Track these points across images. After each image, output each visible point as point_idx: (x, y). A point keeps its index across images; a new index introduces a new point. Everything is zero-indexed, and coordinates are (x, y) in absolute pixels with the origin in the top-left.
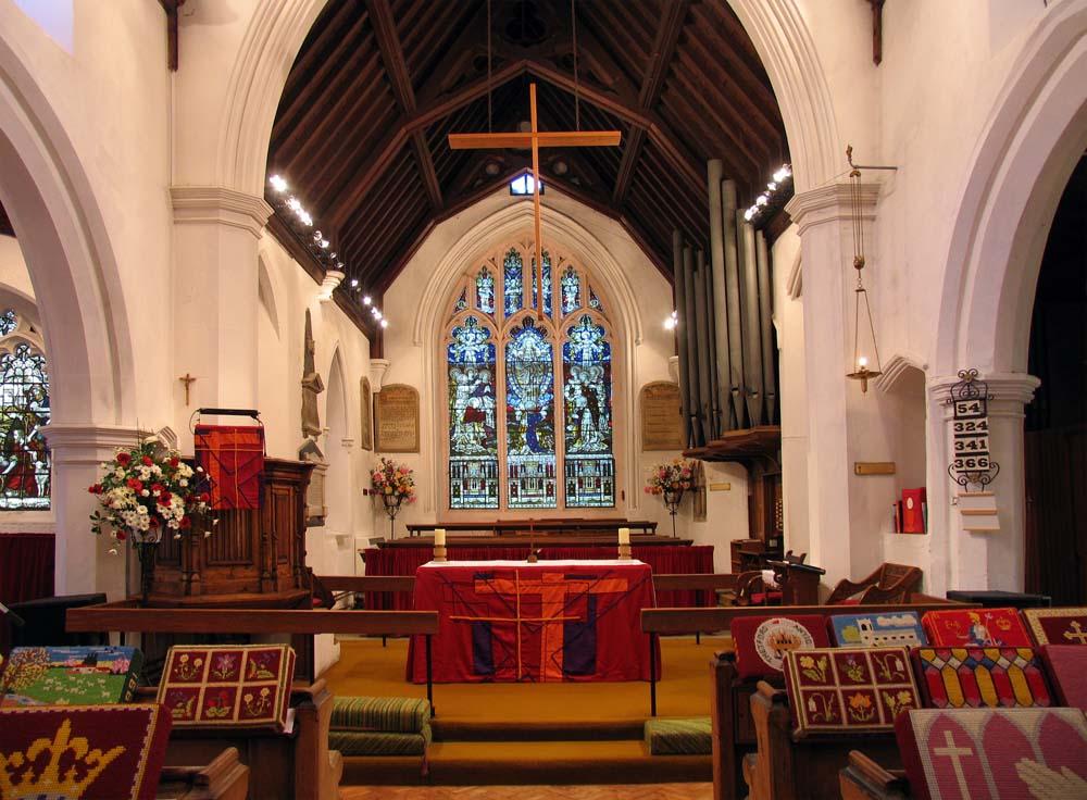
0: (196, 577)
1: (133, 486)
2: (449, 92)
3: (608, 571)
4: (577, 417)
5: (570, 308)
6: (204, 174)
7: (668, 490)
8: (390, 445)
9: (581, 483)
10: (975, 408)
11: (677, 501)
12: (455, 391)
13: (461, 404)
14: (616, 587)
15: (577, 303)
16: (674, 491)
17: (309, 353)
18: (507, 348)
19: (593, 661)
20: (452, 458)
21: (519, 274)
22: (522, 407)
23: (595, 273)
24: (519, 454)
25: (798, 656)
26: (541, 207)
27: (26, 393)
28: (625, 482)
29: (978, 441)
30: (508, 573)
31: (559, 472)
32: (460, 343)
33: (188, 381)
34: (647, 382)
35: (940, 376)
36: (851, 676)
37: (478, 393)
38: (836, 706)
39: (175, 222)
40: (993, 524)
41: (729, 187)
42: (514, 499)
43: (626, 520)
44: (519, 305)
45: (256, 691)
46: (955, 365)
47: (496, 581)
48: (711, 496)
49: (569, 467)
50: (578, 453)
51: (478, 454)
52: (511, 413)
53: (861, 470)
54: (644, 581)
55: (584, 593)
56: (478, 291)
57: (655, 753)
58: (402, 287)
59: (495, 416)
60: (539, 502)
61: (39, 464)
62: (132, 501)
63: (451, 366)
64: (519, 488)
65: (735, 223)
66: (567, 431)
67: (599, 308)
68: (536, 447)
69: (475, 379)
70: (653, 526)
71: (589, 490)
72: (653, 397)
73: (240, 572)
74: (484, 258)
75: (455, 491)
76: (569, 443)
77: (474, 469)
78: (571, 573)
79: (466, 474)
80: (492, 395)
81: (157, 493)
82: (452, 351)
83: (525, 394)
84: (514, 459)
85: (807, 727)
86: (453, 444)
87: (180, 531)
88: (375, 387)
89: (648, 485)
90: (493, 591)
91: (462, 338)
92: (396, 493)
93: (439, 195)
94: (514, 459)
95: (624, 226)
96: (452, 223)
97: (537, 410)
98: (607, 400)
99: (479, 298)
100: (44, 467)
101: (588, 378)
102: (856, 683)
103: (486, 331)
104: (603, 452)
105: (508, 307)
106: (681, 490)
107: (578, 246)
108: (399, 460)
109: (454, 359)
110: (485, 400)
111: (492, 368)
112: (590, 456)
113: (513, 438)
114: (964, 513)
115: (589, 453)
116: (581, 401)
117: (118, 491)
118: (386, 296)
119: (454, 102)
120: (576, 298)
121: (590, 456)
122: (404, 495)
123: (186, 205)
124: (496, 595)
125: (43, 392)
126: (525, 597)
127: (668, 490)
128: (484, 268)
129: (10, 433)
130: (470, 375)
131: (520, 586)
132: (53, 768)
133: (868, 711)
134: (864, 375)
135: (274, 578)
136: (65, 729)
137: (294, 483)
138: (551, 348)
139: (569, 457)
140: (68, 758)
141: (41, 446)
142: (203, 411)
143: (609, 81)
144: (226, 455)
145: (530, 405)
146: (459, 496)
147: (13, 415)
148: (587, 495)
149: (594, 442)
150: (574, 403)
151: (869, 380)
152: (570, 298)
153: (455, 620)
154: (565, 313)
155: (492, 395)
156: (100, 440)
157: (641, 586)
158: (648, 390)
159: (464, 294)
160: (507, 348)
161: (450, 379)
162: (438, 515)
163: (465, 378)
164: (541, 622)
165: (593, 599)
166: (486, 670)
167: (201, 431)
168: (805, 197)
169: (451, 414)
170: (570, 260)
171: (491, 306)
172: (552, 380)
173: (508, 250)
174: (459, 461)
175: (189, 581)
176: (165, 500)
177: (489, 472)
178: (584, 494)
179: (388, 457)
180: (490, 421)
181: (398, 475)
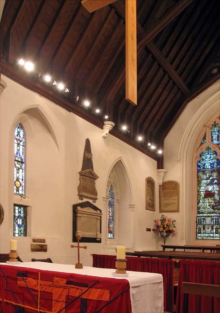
8: (166, 209)
12: (200, 183)
14: (101, 296)
20: (198, 215)
23: (168, 104)
32: (203, 160)
54: (122, 294)
56: (212, 134)
58: (171, 138)
63: (198, 171)
69: (210, 176)
74: (214, 117)
75: (199, 230)
77: (208, 220)
86: (199, 208)
90: (26, 286)
91: (204, 157)
99: (212, 137)
103: (216, 153)
108: (168, 216)
109: (200, 168)
110: (215, 187)
124: (27, 289)
126: (43, 293)
130: (208, 175)
131: (41, 285)
146: (200, 233)
153: (7, 302)
159: (205, 136)
161: (198, 177)
162: (186, 242)
163: (205, 177)
165: (85, 302)
171: (218, 140)
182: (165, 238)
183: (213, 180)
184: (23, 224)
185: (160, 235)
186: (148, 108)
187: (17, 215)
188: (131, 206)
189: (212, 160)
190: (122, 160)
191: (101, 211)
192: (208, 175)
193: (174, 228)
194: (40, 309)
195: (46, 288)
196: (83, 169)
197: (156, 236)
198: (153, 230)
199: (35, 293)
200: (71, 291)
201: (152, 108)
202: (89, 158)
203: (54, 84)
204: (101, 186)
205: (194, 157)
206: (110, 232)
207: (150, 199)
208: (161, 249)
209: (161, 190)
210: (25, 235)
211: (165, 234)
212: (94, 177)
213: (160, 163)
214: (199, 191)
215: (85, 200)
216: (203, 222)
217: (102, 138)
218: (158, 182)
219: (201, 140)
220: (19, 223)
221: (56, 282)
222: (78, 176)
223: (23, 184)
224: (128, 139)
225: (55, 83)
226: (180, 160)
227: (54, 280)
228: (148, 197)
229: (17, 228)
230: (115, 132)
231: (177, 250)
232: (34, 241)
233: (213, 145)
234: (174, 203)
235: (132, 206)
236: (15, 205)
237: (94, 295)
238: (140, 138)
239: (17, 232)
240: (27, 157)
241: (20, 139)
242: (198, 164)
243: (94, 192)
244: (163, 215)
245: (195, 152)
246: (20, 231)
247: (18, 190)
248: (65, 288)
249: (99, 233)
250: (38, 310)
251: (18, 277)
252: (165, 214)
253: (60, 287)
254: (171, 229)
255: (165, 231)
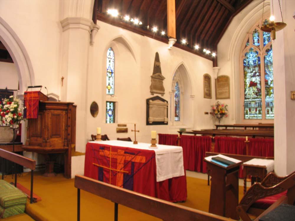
14: (141, 160)
24: (270, 98)
32: (248, 58)
42: (268, 115)
51: (254, 98)
54: (152, 158)
55: (130, 161)
56: (253, 38)
58: (222, 44)
59: (260, 84)
63: (244, 67)
64: (270, 111)
69: (253, 70)
75: (246, 112)
77: (253, 104)
79: (250, 106)
80: (259, 75)
82: (245, 61)
96: (239, 15)
99: (254, 40)
103: (257, 52)
105: (264, 42)
108: (222, 102)
109: (246, 64)
111: (259, 66)
126: (113, 159)
128: (255, 29)
130: (251, 69)
142: (29, 87)
148: (253, 114)
155: (259, 75)
157: (151, 160)
161: (244, 71)
162: (236, 122)
163: (249, 71)
164: (116, 171)
165: (133, 164)
171: (258, 43)
173: (264, 21)
174: (247, 101)
177: (259, 105)
180: (259, 86)
182: (219, 119)
183: (256, 73)
184: (112, 114)
185: (216, 118)
186: (203, 24)
187: (108, 108)
188: (191, 97)
189: (254, 58)
190: (184, 64)
191: (167, 102)
192: (251, 69)
193: (226, 112)
194: (111, 168)
195: (114, 156)
196: (154, 73)
197: (213, 118)
198: (211, 113)
199: (108, 159)
200: (127, 157)
201: (206, 23)
202: (158, 65)
203: (131, 21)
204: (168, 84)
205: (241, 56)
206: (176, 116)
207: (207, 90)
208: (215, 128)
209: (216, 83)
210: (114, 122)
211: (219, 116)
212: (162, 79)
213: (215, 62)
214: (245, 82)
215: (155, 95)
216: (249, 105)
217: (168, 51)
218: (213, 77)
219: (245, 43)
220: (109, 114)
221: (119, 152)
222: (151, 79)
223: (113, 87)
224: (189, 48)
225: (132, 20)
226: (230, 59)
227: (118, 151)
228: (206, 89)
229: (108, 117)
230: (178, 44)
231: (228, 128)
232: (119, 125)
233: (255, 47)
234: (226, 92)
235: (192, 97)
236: (107, 102)
237: (138, 159)
238: (197, 47)
239: (108, 120)
240: (115, 69)
241: (111, 58)
242: (244, 61)
243: (162, 89)
244: (218, 102)
245: (241, 53)
246: (111, 119)
247: (109, 92)
248: (124, 155)
249: (166, 118)
250: (110, 169)
251: (100, 150)
252: (219, 100)
253: (121, 155)
254: (223, 112)
255: (219, 113)
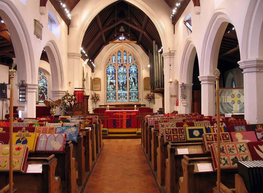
0: (74, 112)
1: (67, 99)
2: (108, 26)
3: (133, 112)
4: (131, 84)
5: (130, 62)
6: (73, 51)
7: (148, 98)
8: (95, 89)
9: (132, 97)
10: (184, 88)
11: (150, 101)
12: (108, 79)
13: (109, 81)
15: (132, 61)
16: (150, 98)
17: (83, 74)
18: (118, 70)
19: (130, 125)
20: (107, 92)
21: (120, 55)
22: (121, 82)
25: (165, 129)
26: (124, 45)
27: (44, 84)
28: (140, 97)
29: (184, 93)
30: (118, 112)
31: (128, 94)
32: (109, 69)
33: (70, 83)
34: (145, 77)
35: (180, 83)
36: (174, 133)
37: (112, 79)
38: (171, 138)
39: (68, 58)
40: (185, 104)
41: (157, 46)
42: (119, 100)
43: (140, 104)
44: (120, 61)
45: (95, 120)
46: (182, 82)
47: (117, 113)
48: (156, 99)
49: (130, 93)
50: (131, 91)
51: (112, 91)
52: (119, 83)
53: (171, 96)
57: (137, 135)
58: (97, 59)
59: (115, 83)
60: (124, 101)
61: (45, 95)
62: (67, 101)
63: (107, 74)
65: (157, 52)
66: (129, 86)
67: (136, 62)
68: (123, 90)
69: (112, 76)
70: (145, 105)
71: (134, 98)
72: (146, 80)
73: (80, 112)
76: (130, 89)
77: (111, 94)
78: (127, 112)
80: (115, 79)
81: (70, 100)
82: (107, 71)
83: (121, 79)
84: (119, 92)
85: (166, 141)
86: (107, 89)
87: (73, 106)
88: (93, 78)
89: (145, 97)
92: (97, 99)
93: (105, 40)
94: (119, 92)
95: (140, 46)
97: (124, 82)
98: (137, 80)
99: (113, 60)
100: (46, 96)
101: (134, 76)
102: (175, 134)
103: (114, 67)
104: (136, 91)
105: (118, 62)
106: (151, 98)
107: (132, 50)
111: (115, 74)
112: (134, 92)
113: (119, 88)
114: (182, 103)
115: (134, 91)
116: (132, 81)
117: (66, 100)
118: (95, 60)
119: (109, 28)
120: (132, 60)
121: (134, 92)
122: (98, 99)
123: (70, 55)
124: (116, 115)
125: (46, 84)
127: (148, 98)
129: (41, 91)
130: (111, 75)
132: (87, 122)
133: (177, 138)
134: (171, 82)
135: (85, 113)
136: (87, 119)
137: (87, 99)
138: (126, 70)
139: (130, 92)
140: (87, 121)
141: (46, 93)
142: (75, 88)
143: (136, 24)
144: (78, 95)
145: (122, 81)
146: (108, 99)
147: (42, 88)
149: (135, 89)
150: (131, 81)
151: (172, 83)
152: (130, 60)
154: (129, 63)
155: (115, 79)
156: (60, 92)
158: (145, 79)
160: (118, 70)
161: (107, 76)
165: (131, 116)
166: (115, 126)
167: (75, 91)
168: (164, 54)
169: (107, 83)
170: (130, 53)
172: (127, 76)
175: (73, 113)
176: (72, 102)
178: (133, 99)
179: (95, 92)
180: (114, 85)
181: (97, 95)
